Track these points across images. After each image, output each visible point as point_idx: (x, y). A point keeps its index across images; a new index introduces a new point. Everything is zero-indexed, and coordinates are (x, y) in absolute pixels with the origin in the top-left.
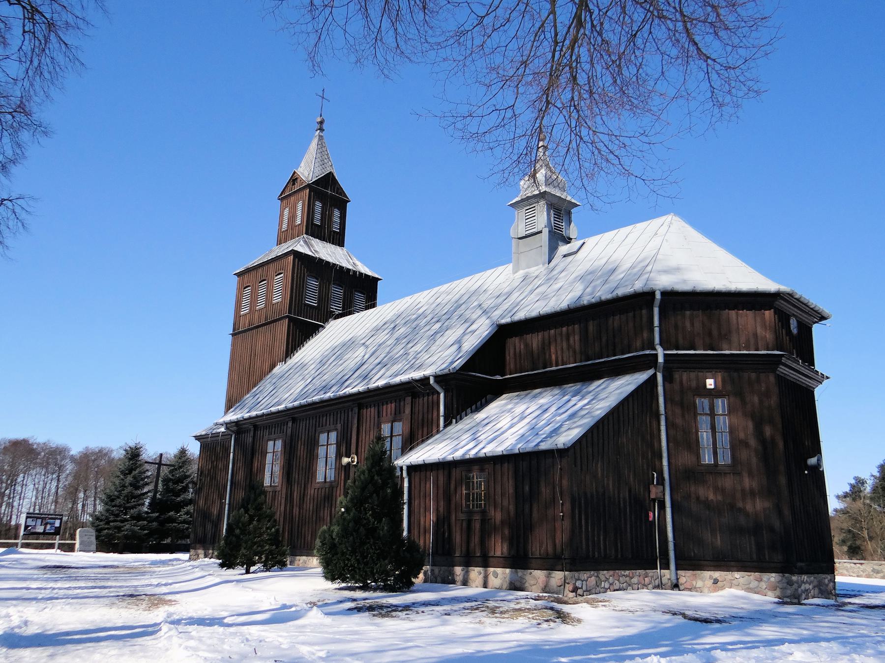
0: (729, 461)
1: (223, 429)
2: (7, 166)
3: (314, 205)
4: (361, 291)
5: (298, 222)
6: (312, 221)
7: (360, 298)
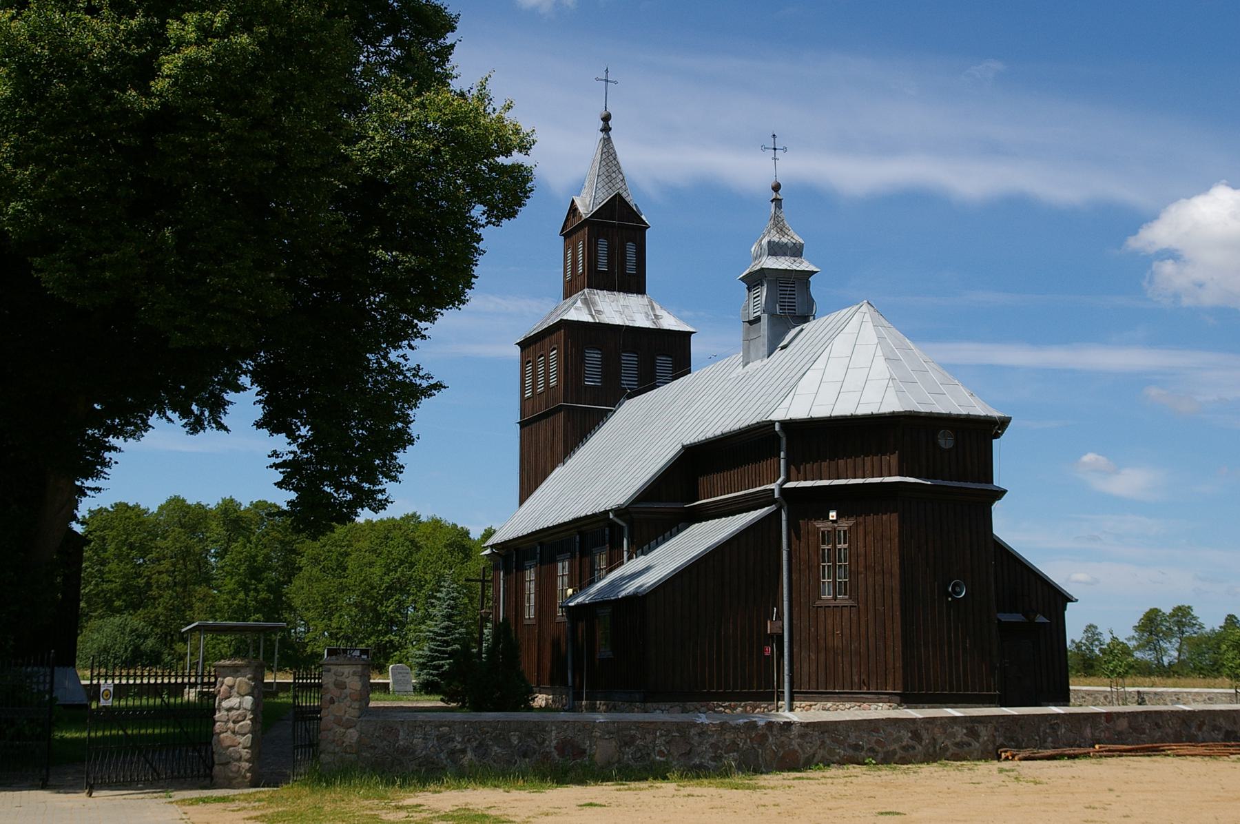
1: (169, 413)
3: (596, 244)
4: (664, 356)
6: (596, 267)
7: (663, 362)
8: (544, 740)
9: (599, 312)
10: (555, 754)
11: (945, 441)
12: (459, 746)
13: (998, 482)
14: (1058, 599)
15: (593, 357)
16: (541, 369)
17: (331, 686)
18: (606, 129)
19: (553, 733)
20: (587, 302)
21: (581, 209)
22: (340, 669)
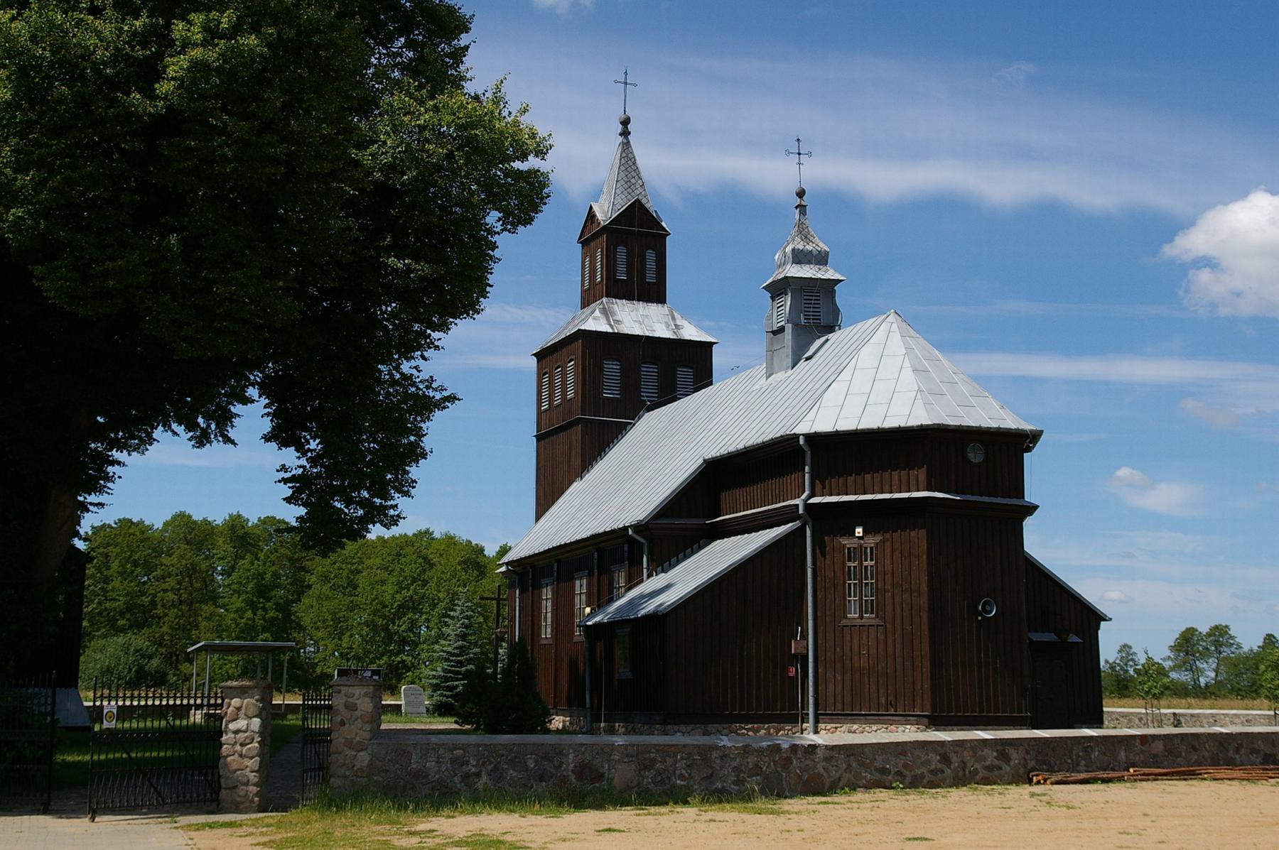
8: (562, 763)
9: (617, 322)
10: (573, 778)
11: (975, 455)
12: (473, 770)
13: (1030, 497)
14: (1091, 618)
15: (612, 368)
16: (558, 381)
17: (342, 708)
18: (625, 133)
19: (571, 757)
20: (606, 312)
21: (600, 216)
22: (351, 690)
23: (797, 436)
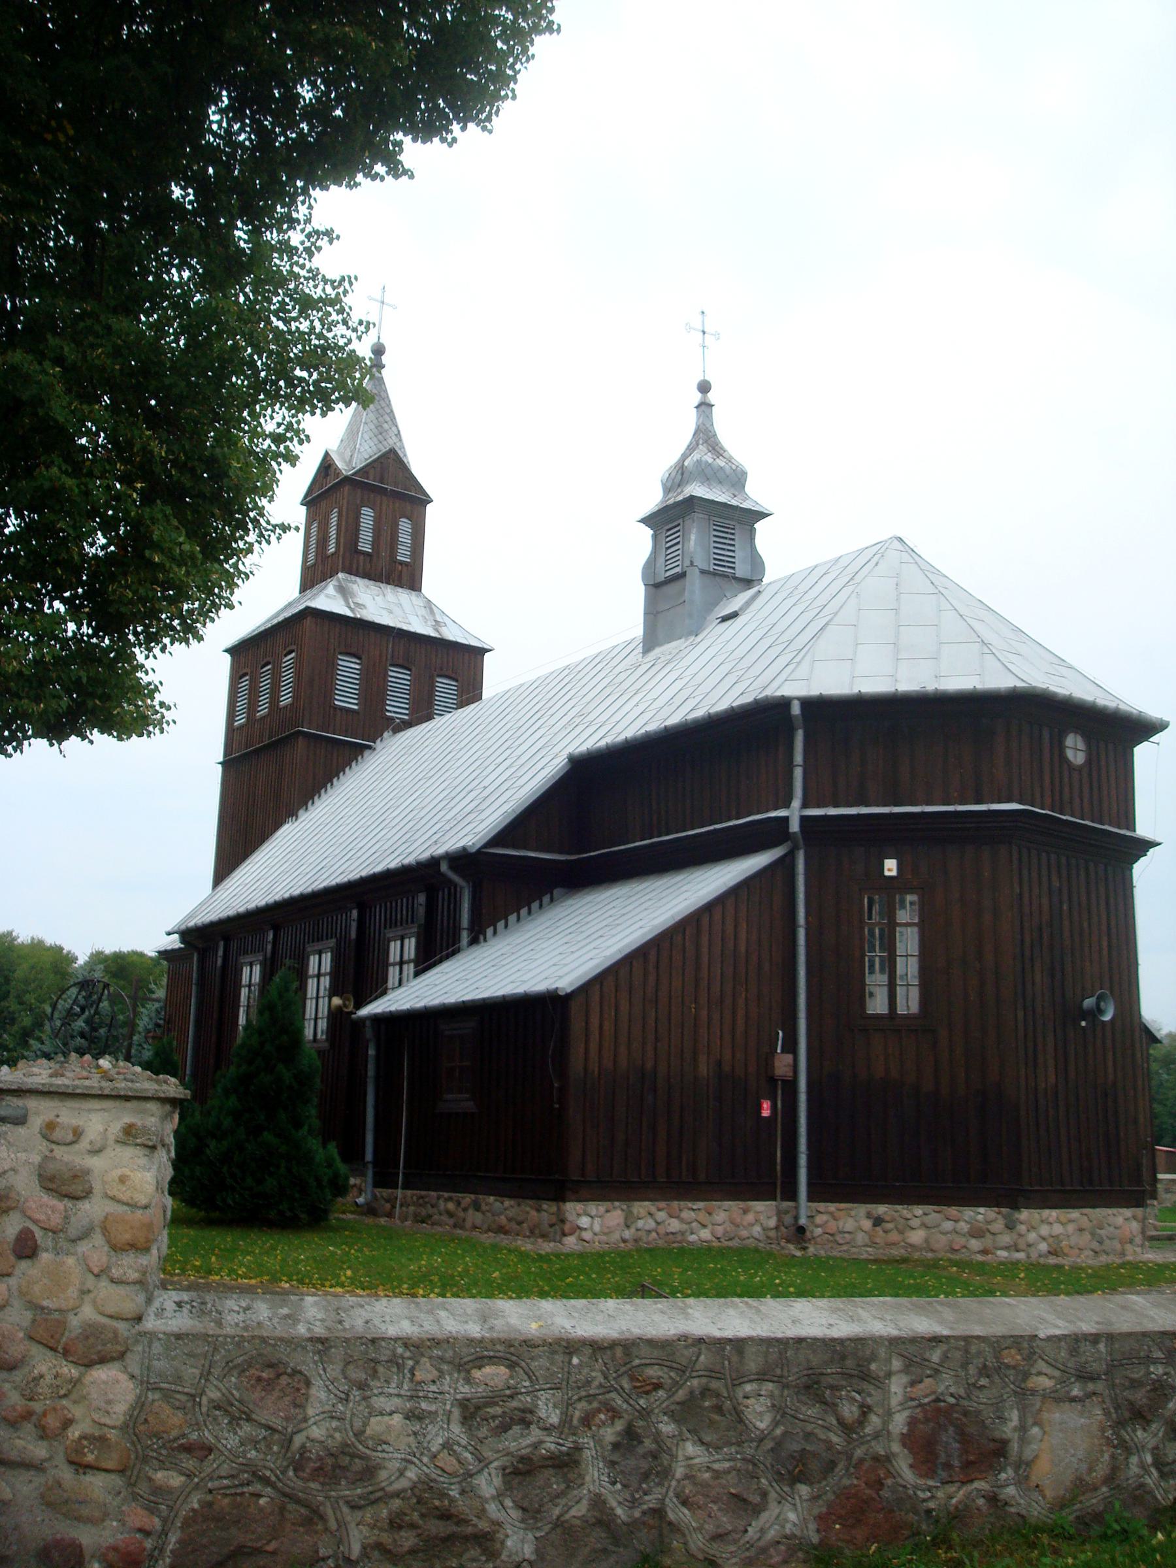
0: (914, 1008)
2: (43, 1423)
5: (332, 549)
9: (358, 605)
10: (904, 1468)
12: (550, 1444)
15: (348, 667)
19: (897, 1387)
20: (343, 591)
22: (67, 1115)
23: (783, 704)
